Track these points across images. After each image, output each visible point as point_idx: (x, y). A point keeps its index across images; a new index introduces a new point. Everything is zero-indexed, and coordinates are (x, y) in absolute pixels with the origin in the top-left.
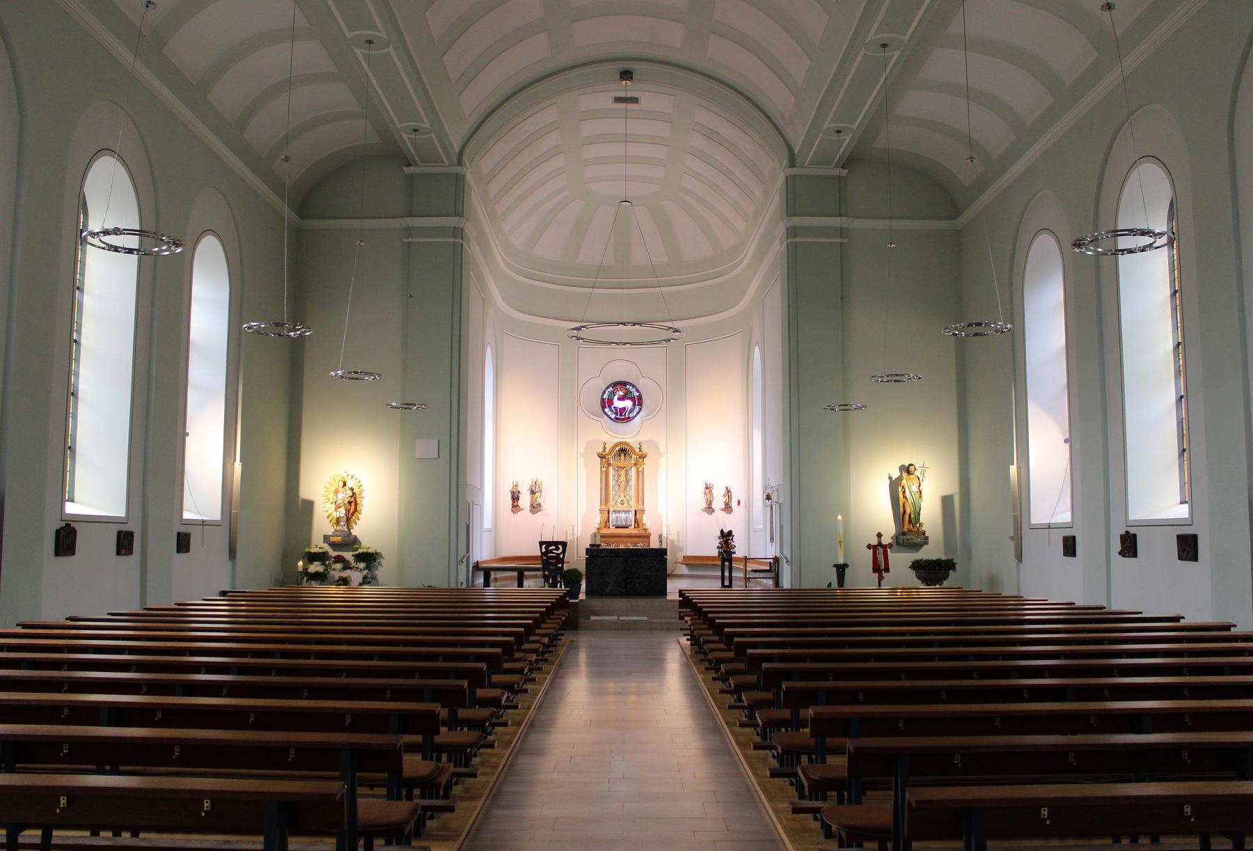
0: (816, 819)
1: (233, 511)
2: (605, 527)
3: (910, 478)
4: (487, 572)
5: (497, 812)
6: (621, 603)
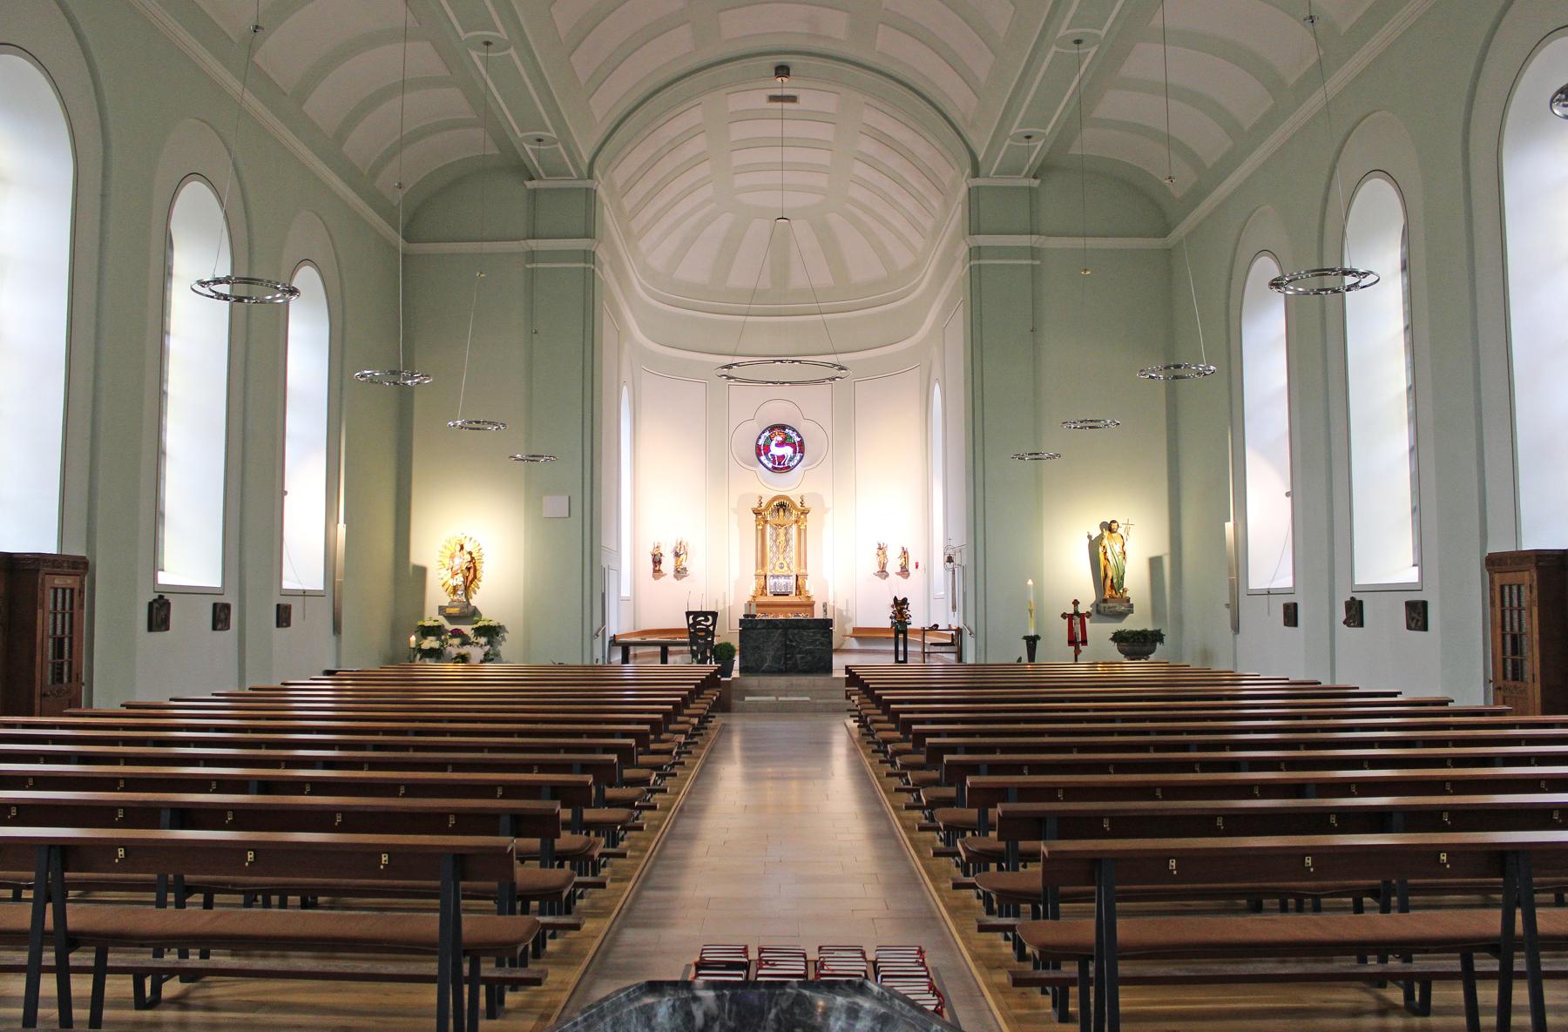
1: (337, 580)
2: (761, 595)
3: (1112, 537)
4: (625, 648)
6: (780, 681)
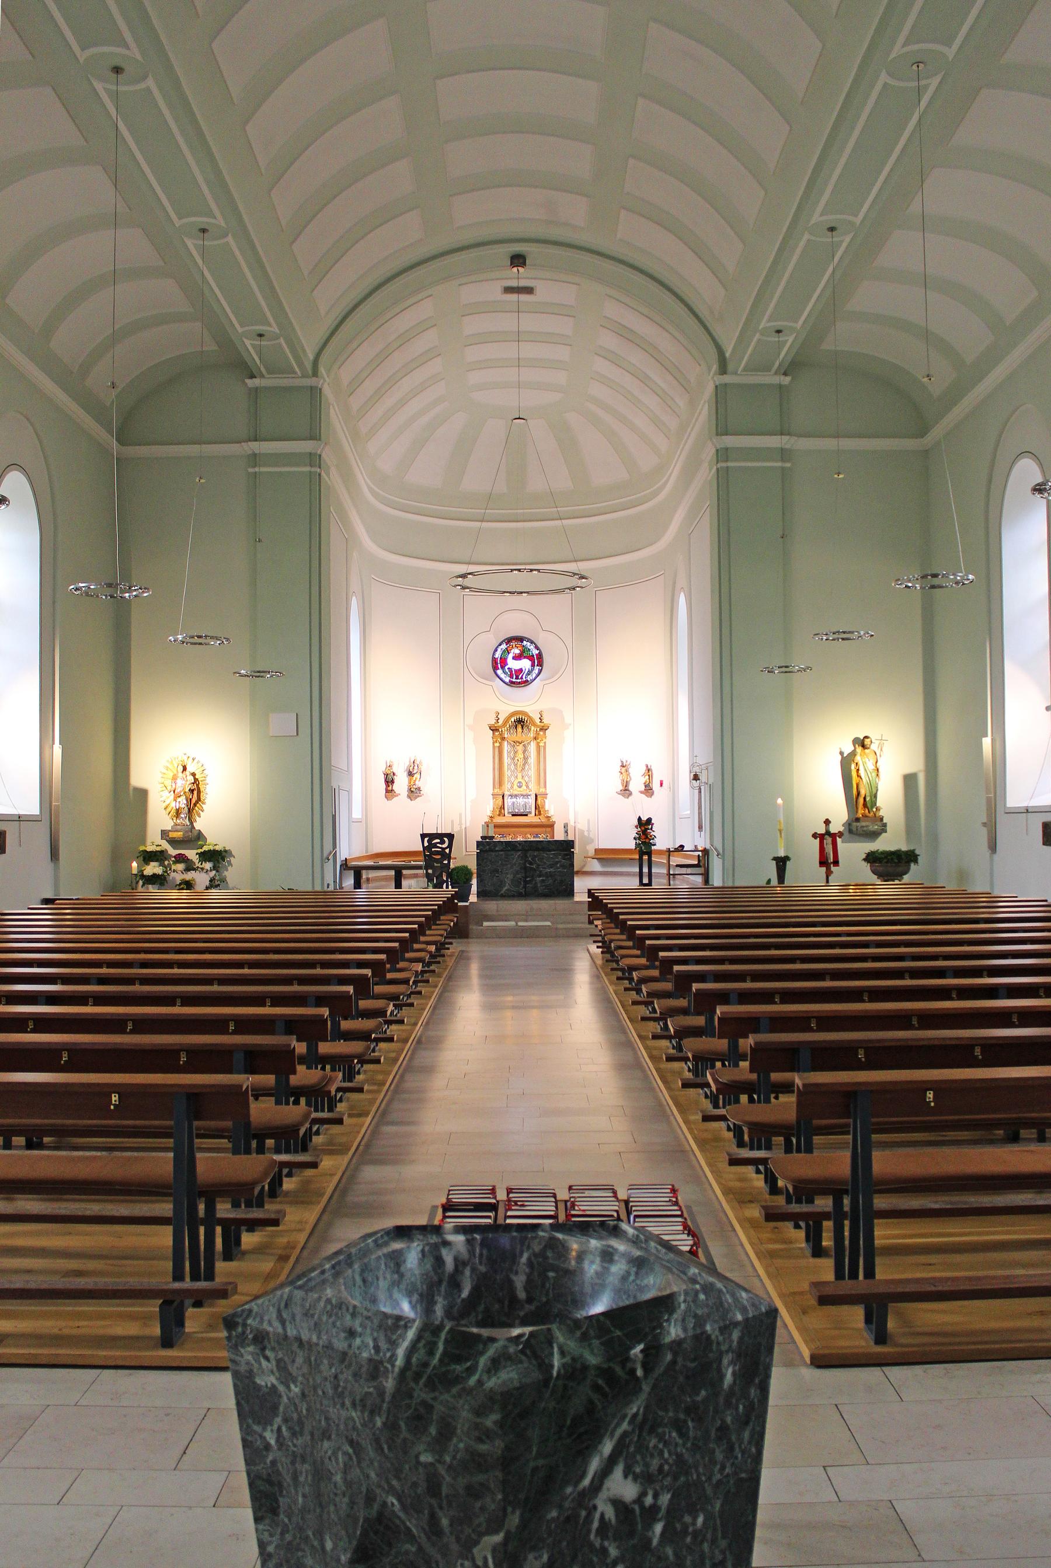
0: (758, 1172)
2: (499, 815)
4: (358, 872)
5: (451, 983)
6: (520, 906)
